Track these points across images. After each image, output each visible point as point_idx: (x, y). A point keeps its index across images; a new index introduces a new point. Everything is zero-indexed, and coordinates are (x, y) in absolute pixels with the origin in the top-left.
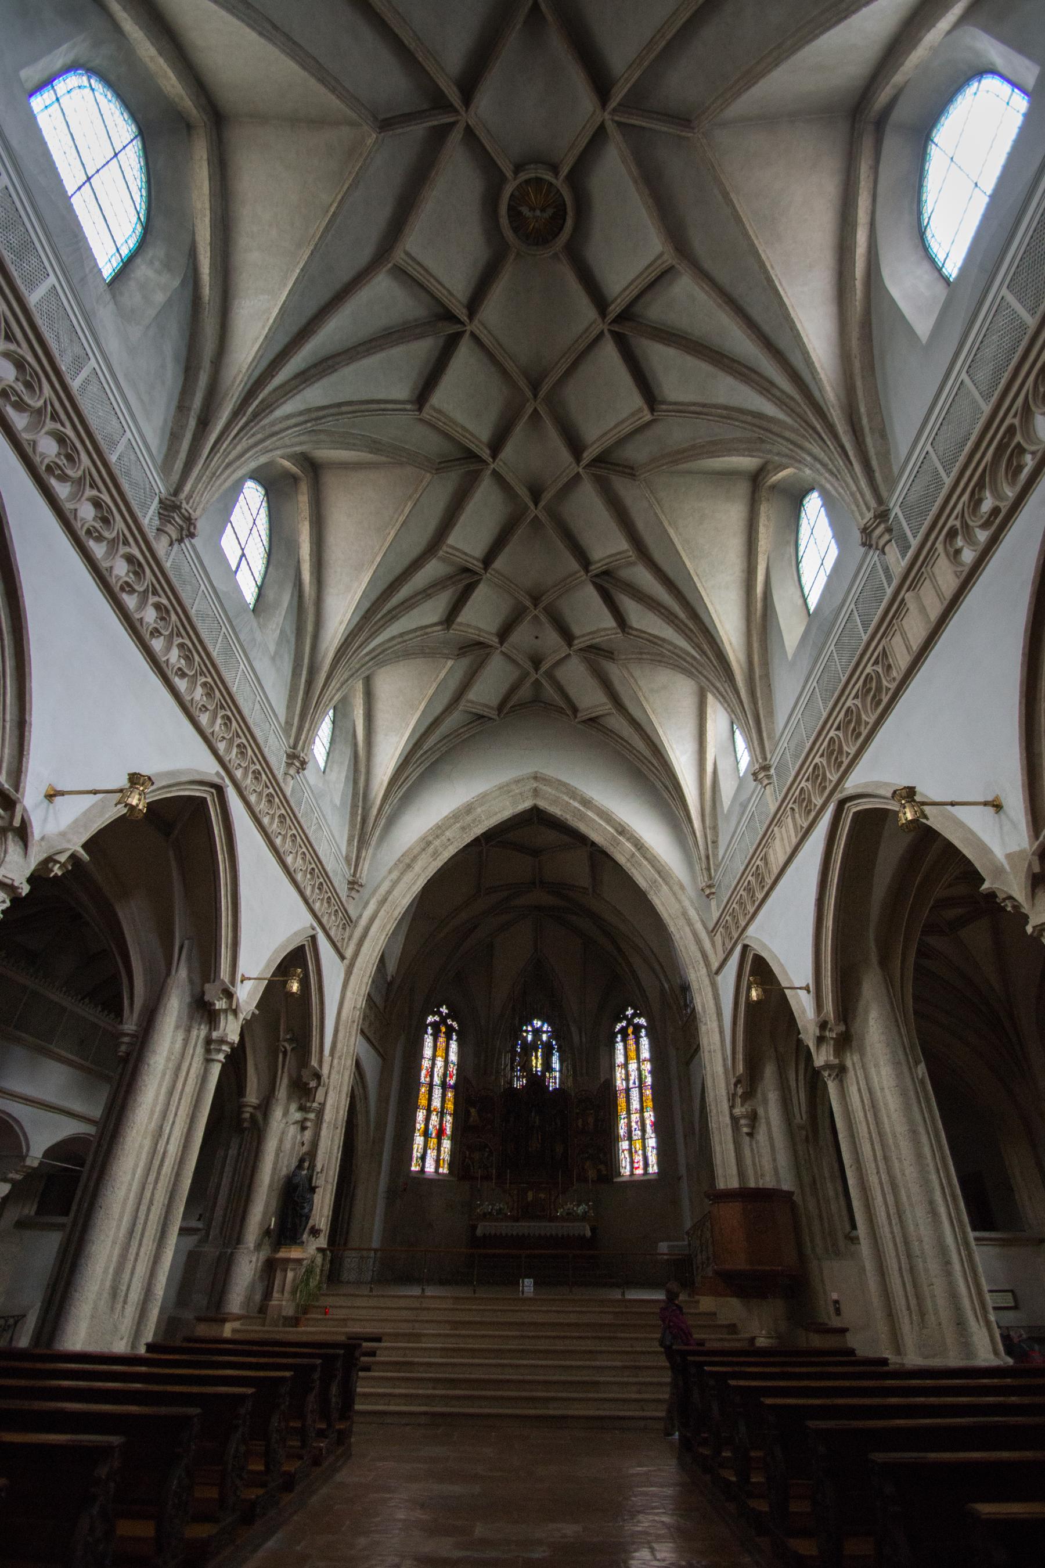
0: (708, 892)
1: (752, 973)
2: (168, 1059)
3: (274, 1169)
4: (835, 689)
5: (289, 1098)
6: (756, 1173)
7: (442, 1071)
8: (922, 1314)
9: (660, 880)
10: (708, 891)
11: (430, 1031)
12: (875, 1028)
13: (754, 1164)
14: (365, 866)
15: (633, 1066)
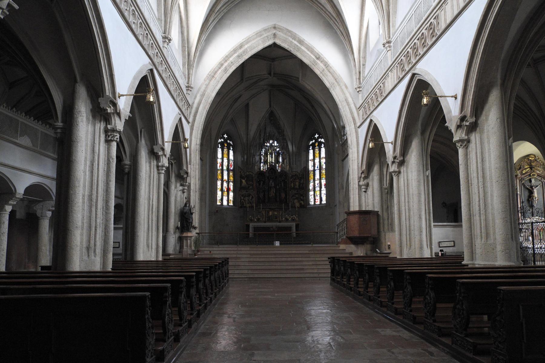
0: (358, 90)
1: (371, 137)
2: (146, 174)
3: (175, 207)
4: (420, 21)
5: (176, 181)
6: (366, 205)
7: (227, 164)
8: (410, 246)
9: (336, 83)
10: (359, 90)
11: (220, 146)
12: (414, 157)
13: (365, 202)
14: (192, 78)
15: (317, 161)
